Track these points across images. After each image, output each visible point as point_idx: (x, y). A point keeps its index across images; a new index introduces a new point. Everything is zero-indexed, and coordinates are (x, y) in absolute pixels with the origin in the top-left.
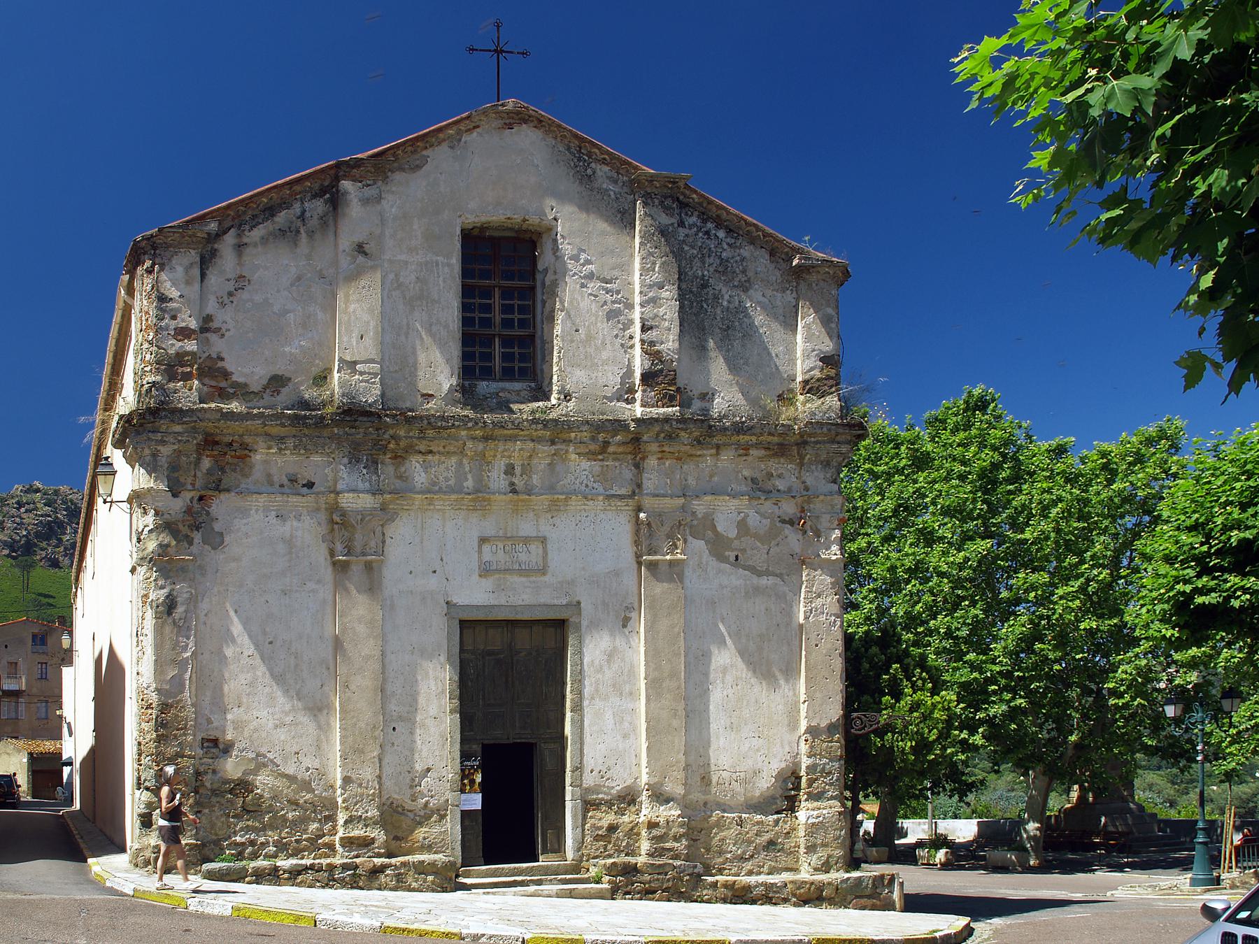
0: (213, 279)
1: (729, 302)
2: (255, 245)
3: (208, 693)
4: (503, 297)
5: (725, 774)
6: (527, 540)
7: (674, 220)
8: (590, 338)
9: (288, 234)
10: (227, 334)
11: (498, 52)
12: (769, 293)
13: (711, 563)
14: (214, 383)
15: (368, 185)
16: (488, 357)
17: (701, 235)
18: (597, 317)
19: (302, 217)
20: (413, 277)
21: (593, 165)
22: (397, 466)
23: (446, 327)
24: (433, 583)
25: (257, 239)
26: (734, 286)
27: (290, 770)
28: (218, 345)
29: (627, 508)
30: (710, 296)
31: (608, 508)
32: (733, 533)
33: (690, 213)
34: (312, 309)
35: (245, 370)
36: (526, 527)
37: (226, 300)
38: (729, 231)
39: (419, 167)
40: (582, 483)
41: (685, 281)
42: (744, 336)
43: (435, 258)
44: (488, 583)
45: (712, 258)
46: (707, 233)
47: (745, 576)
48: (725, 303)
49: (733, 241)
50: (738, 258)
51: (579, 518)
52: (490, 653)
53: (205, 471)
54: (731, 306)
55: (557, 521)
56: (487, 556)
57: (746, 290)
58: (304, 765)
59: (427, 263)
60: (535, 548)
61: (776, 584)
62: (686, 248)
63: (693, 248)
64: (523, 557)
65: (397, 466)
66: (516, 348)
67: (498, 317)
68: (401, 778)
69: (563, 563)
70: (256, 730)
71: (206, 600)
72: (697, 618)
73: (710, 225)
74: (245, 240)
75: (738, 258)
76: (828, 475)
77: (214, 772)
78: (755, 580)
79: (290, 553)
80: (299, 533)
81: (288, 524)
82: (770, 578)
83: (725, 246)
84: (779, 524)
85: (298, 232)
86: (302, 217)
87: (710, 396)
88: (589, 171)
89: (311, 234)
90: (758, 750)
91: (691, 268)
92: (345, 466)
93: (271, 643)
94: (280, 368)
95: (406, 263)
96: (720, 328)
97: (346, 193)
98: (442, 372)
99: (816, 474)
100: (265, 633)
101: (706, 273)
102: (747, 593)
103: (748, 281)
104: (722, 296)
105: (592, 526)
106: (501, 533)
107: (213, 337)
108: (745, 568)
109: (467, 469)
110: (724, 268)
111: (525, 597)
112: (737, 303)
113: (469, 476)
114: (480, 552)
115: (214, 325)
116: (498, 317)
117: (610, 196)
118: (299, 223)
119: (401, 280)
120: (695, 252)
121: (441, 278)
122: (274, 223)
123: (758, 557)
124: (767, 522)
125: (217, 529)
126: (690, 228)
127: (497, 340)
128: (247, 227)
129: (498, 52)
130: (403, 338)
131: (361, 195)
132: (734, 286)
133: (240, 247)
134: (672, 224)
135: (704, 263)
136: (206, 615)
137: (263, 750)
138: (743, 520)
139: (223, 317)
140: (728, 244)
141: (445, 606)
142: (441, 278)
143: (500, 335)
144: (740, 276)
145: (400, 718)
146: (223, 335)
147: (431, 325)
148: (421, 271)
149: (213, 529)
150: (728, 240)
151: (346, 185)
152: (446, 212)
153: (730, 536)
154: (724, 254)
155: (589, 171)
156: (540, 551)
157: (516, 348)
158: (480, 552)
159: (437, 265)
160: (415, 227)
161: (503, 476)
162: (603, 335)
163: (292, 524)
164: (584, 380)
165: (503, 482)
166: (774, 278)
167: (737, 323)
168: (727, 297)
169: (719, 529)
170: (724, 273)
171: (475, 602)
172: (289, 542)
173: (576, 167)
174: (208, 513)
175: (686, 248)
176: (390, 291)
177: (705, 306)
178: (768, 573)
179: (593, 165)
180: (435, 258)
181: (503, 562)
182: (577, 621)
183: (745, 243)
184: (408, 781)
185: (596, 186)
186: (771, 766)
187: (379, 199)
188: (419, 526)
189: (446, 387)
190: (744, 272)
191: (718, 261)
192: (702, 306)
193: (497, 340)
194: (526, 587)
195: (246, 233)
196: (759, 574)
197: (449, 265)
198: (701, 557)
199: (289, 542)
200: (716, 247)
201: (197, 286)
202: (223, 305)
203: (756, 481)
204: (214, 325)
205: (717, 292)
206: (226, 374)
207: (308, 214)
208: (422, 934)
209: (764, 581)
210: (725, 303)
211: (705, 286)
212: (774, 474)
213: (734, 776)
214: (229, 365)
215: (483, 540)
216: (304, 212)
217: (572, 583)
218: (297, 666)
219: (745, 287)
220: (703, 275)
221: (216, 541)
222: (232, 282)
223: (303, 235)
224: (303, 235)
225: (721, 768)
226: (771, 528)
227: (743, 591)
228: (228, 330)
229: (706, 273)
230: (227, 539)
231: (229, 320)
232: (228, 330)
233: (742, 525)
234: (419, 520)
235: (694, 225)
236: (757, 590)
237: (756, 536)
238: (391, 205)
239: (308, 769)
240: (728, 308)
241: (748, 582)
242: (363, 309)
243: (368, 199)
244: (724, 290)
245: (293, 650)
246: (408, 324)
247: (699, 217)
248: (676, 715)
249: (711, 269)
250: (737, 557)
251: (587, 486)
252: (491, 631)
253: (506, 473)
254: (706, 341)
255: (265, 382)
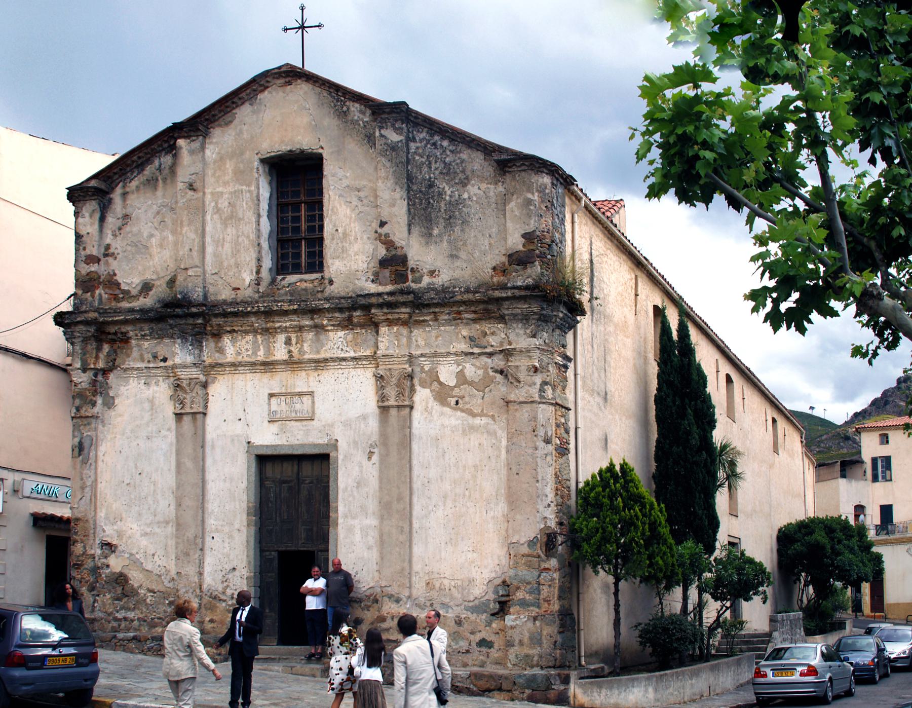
0: (111, 220)
1: (451, 196)
2: (133, 193)
3: (104, 511)
4: (307, 210)
5: (446, 582)
6: (300, 394)
7: (402, 138)
8: (345, 234)
9: (152, 183)
10: (118, 256)
11: (302, 27)
12: (484, 186)
13: (435, 407)
14: (111, 292)
15: (194, 141)
16: (298, 255)
17: (429, 146)
18: (351, 218)
19: (159, 169)
20: (227, 203)
21: (347, 103)
22: (217, 343)
23: (248, 237)
24: (239, 428)
25: (134, 188)
26: (456, 183)
27: (149, 567)
28: (114, 265)
29: (371, 366)
30: (436, 194)
31: (357, 366)
32: (452, 383)
33: (421, 130)
34: (165, 234)
35: (127, 281)
36: (301, 387)
37: (118, 233)
38: (452, 141)
39: (231, 122)
40: (338, 348)
41: (416, 184)
42: (463, 222)
43: (240, 187)
44: (274, 428)
45: (438, 164)
46: (434, 144)
47: (463, 417)
48: (447, 198)
49: (454, 148)
50: (458, 161)
51: (337, 375)
52: (285, 482)
53: (105, 354)
54: (453, 200)
55: (321, 378)
56: (274, 407)
57: (464, 185)
58: (157, 564)
59: (235, 191)
60: (306, 400)
61: (488, 423)
62: (417, 158)
63: (422, 157)
64: (298, 406)
65: (217, 343)
66: (290, 249)
67: (303, 226)
68: (216, 575)
69: (325, 410)
70: (130, 537)
71: (104, 445)
72: (424, 452)
73: (436, 138)
74: (128, 189)
75: (458, 161)
76: (528, 331)
77: (108, 566)
78: (471, 420)
79: (152, 409)
80: (157, 395)
81: (151, 389)
82: (483, 418)
83: (448, 153)
84: (492, 374)
85: (157, 180)
86: (159, 169)
87: (437, 273)
88: (345, 109)
89: (165, 180)
90: (473, 562)
91: (421, 172)
92: (179, 344)
93: (140, 474)
94: (149, 276)
95: (222, 193)
96: (444, 218)
97: (181, 148)
98: (245, 271)
99: (517, 331)
100: (136, 467)
101: (432, 175)
102: (464, 431)
103: (467, 178)
104: (445, 192)
105: (347, 381)
106: (284, 391)
107: (110, 260)
108: (463, 411)
109: (260, 342)
110: (448, 171)
111: (299, 437)
112: (457, 196)
113: (261, 347)
114: (269, 404)
115: (111, 251)
116: (303, 226)
117: (359, 125)
118: (158, 173)
119: (219, 206)
120: (424, 160)
121: (244, 202)
122: (143, 175)
123: (476, 401)
124: (480, 372)
125: (111, 395)
126: (421, 141)
127: (303, 243)
128: (128, 180)
129: (302, 27)
130: (220, 249)
131: (189, 148)
132: (456, 183)
133: (125, 195)
134: (401, 141)
135: (430, 168)
136: (104, 455)
137: (134, 552)
138: (462, 371)
139: (117, 245)
140: (450, 151)
141: (246, 445)
142: (244, 202)
143: (305, 239)
144: (460, 175)
145: (217, 531)
146: (116, 258)
147: (238, 237)
148: (232, 198)
149: (109, 394)
150: (451, 148)
151: (181, 142)
152: (248, 153)
153: (450, 385)
154: (447, 160)
155: (345, 109)
156: (310, 402)
157: (290, 249)
158: (269, 404)
159: (242, 192)
160: (228, 166)
161: (284, 346)
162: (355, 232)
163: (154, 388)
164: (341, 268)
165: (283, 350)
166: (488, 174)
167: (457, 213)
168: (449, 193)
169: (442, 380)
170: (447, 174)
171: (266, 443)
172: (151, 401)
173: (335, 106)
174: (107, 384)
175: (417, 158)
176: (212, 215)
177: (431, 201)
178: (482, 415)
179: (347, 103)
180: (240, 187)
181: (285, 411)
182: (335, 455)
183: (464, 148)
184: (220, 577)
185: (350, 118)
186: (483, 576)
187: (203, 148)
188: (230, 386)
189: (247, 281)
190: (463, 171)
191: (443, 165)
192: (429, 202)
193: (303, 243)
194: (299, 430)
195: (128, 184)
196: (474, 415)
197: (249, 191)
198: (427, 403)
199: (151, 401)
200: (441, 154)
201: (96, 226)
202: (115, 236)
203: (473, 339)
204: (111, 251)
205: (441, 190)
206: (118, 285)
207: (163, 166)
208: (204, 706)
209: (477, 421)
210: (447, 198)
211: (431, 185)
212: (488, 333)
213: (453, 583)
214: (119, 278)
215: (271, 395)
216: (160, 166)
217: (332, 425)
218: (154, 491)
219: (464, 183)
220: (430, 178)
221: (110, 403)
222: (121, 220)
223: (160, 182)
224: (160, 182)
225: (442, 576)
226: (484, 377)
227: (461, 429)
228: (118, 254)
229: (432, 175)
230: (116, 402)
231: (119, 247)
232: (118, 254)
233: (461, 375)
234: (230, 382)
235: (424, 139)
236: (473, 428)
237: (471, 383)
238: (211, 152)
239: (159, 566)
240: (450, 201)
241: (465, 422)
242: (191, 231)
243: (193, 150)
244: (447, 188)
245: (153, 479)
246: (224, 238)
247: (427, 133)
248: (402, 531)
249: (437, 172)
250: (457, 403)
251: (342, 350)
252: (285, 465)
253: (286, 344)
254: (432, 229)
255: (139, 288)
